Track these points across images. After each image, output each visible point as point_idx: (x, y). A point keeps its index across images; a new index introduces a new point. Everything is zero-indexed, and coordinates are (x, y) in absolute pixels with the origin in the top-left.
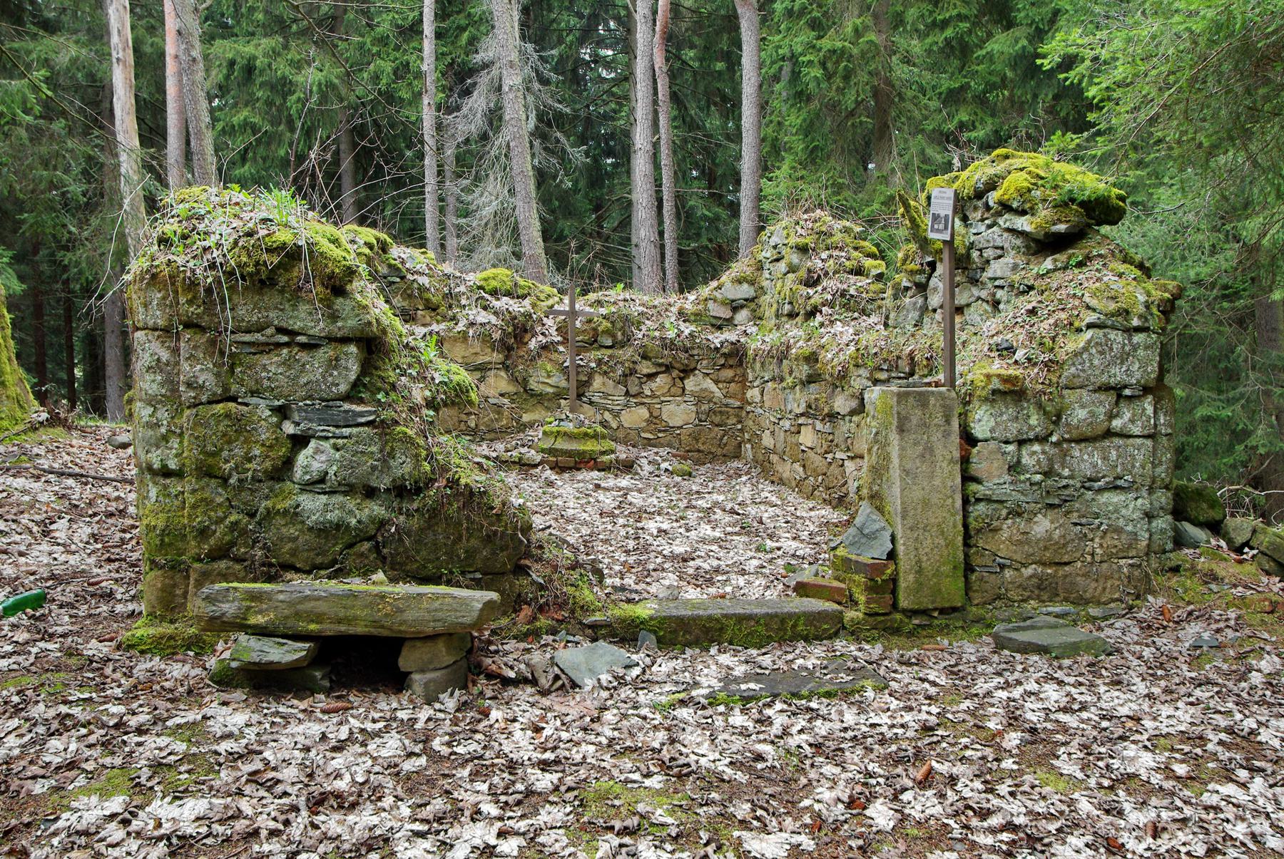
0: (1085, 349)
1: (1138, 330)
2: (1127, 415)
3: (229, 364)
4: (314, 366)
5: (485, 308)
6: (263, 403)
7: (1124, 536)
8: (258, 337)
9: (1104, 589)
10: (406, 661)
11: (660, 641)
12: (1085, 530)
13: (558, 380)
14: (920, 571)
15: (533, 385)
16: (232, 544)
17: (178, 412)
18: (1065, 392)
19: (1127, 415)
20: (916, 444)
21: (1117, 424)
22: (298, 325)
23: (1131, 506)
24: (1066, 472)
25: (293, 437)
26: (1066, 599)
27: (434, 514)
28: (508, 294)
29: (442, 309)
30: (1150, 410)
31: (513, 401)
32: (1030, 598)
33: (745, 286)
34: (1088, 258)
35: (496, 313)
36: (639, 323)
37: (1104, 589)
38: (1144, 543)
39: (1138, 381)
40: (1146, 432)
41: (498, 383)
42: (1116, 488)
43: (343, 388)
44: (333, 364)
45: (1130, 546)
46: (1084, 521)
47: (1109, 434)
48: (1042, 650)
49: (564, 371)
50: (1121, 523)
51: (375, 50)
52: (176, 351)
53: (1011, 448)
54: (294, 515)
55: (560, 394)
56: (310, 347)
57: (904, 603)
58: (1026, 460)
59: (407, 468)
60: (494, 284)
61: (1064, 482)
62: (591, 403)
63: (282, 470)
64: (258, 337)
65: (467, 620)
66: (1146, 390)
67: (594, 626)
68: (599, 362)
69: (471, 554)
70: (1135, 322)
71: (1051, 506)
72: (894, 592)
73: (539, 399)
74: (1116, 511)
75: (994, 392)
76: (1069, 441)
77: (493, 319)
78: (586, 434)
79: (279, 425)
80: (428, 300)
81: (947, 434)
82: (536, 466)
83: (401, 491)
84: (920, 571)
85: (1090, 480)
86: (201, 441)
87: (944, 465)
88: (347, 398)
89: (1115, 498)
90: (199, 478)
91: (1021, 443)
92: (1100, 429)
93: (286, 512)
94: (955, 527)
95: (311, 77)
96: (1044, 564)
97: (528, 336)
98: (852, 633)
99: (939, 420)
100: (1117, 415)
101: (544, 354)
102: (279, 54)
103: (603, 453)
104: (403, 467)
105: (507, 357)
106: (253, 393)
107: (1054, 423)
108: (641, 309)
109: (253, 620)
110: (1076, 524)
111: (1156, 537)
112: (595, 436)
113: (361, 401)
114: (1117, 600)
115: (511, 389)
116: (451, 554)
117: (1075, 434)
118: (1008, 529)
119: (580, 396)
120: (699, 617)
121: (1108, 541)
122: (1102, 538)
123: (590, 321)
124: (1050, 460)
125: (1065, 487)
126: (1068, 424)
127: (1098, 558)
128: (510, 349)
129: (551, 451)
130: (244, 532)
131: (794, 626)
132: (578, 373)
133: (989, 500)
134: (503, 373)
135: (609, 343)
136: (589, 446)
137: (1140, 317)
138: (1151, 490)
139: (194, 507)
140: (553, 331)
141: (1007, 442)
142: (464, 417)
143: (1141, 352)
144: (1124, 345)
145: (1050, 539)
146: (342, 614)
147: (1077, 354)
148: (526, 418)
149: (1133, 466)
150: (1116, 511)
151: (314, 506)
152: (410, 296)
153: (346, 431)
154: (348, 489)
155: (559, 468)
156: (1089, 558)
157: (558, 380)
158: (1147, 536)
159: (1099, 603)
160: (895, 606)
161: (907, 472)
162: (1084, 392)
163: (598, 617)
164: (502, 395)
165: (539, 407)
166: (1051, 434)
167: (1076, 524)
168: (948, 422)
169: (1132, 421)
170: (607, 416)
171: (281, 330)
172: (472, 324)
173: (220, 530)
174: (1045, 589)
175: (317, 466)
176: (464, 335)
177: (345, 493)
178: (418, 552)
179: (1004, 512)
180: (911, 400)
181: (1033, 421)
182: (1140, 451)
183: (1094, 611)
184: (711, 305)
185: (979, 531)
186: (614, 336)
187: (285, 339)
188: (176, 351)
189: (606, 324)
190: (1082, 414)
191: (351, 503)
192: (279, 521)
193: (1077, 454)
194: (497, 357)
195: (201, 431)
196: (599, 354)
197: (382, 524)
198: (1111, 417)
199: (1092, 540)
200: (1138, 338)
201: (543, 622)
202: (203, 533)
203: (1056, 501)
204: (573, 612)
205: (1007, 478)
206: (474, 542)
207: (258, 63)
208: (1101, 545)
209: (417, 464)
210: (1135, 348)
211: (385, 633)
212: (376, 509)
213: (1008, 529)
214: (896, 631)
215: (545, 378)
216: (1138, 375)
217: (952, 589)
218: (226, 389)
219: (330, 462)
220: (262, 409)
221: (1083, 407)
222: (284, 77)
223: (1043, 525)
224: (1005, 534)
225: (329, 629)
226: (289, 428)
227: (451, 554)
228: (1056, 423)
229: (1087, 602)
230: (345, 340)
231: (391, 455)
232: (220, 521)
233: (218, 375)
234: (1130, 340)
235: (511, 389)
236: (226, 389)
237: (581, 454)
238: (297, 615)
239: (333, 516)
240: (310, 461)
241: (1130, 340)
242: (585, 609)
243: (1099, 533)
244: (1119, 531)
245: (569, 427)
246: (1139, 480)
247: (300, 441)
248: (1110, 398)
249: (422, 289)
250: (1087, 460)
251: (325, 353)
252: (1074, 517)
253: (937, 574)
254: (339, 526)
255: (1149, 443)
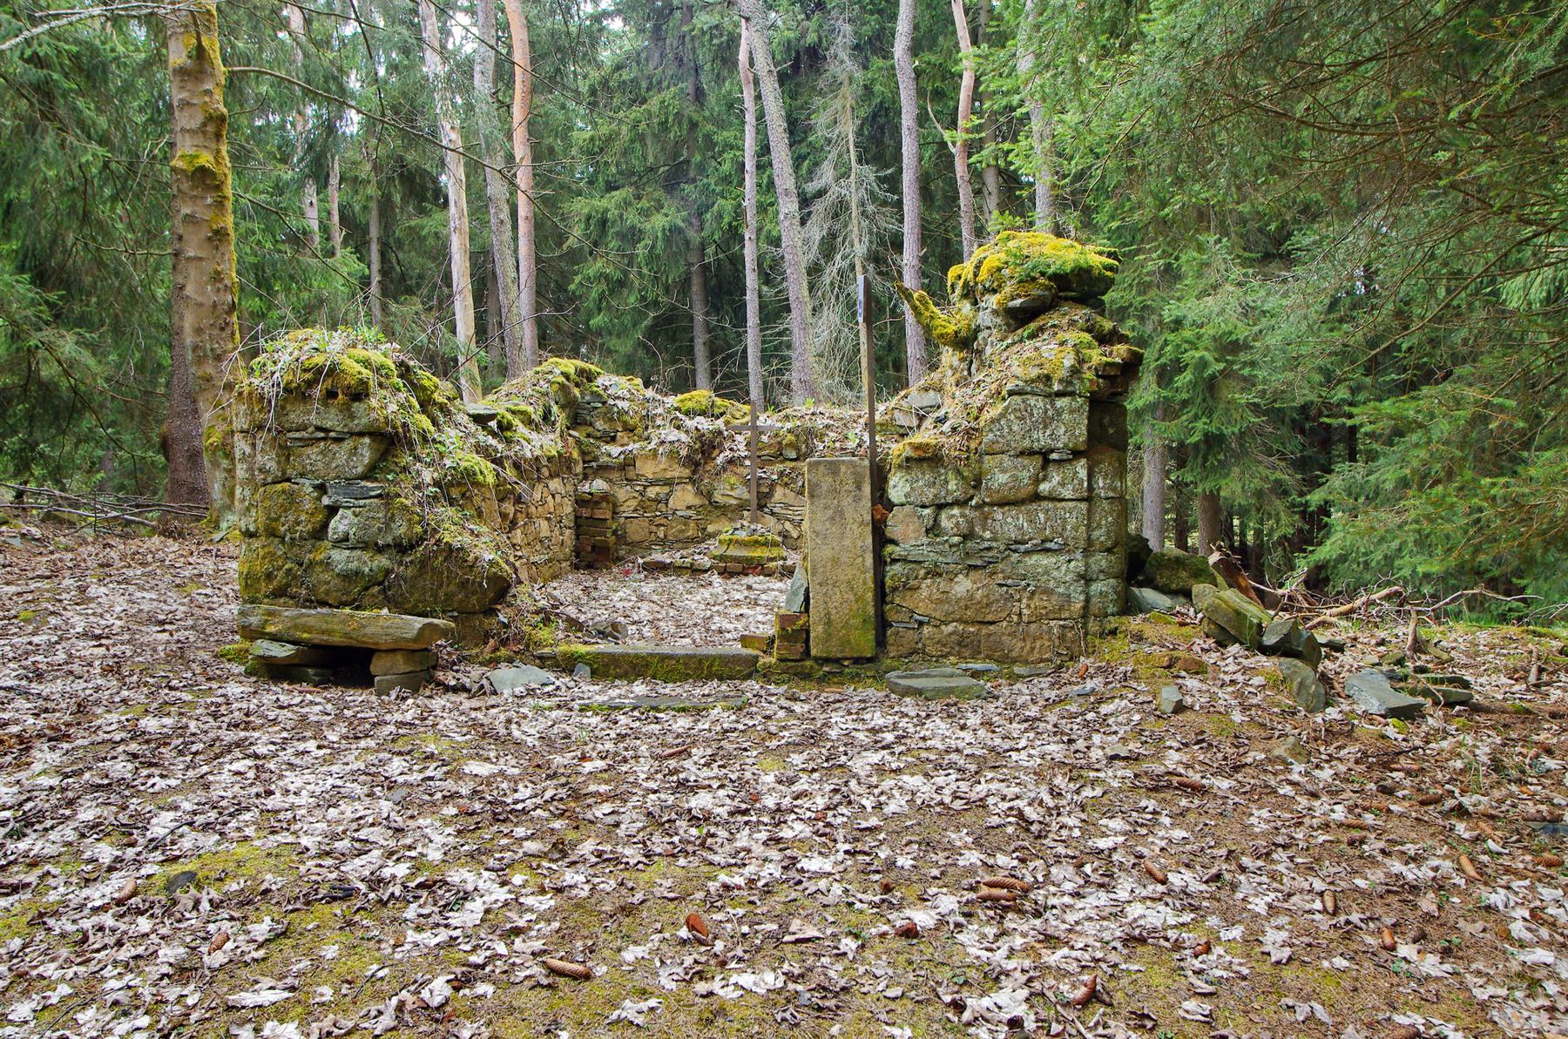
0: (1002, 415)
1: (1060, 394)
2: (1056, 479)
3: (285, 453)
4: (342, 452)
5: (678, 428)
6: (308, 482)
7: (1054, 598)
8: (304, 434)
9: (1033, 649)
10: (377, 666)
11: (593, 673)
12: (1011, 591)
13: (742, 493)
14: (829, 623)
15: (717, 497)
16: (288, 585)
17: (256, 490)
18: (987, 458)
19: (1056, 479)
20: (826, 507)
21: (1044, 487)
22: (329, 424)
23: (1063, 568)
24: (987, 535)
25: (327, 507)
26: (990, 657)
27: (424, 563)
28: (703, 413)
29: (639, 430)
30: (1083, 474)
31: (698, 513)
32: (949, 654)
33: (932, 393)
34: (1041, 329)
35: (687, 432)
36: (822, 435)
37: (1033, 649)
38: (1079, 606)
39: (1066, 445)
40: (1077, 495)
41: (685, 497)
42: (1048, 550)
43: (360, 470)
44: (354, 451)
45: (1061, 608)
46: (1010, 582)
47: (1036, 497)
48: (918, 692)
49: (747, 483)
50: (1052, 584)
51: (718, 189)
52: (254, 445)
53: (927, 511)
54: (327, 564)
55: (742, 506)
56: (338, 440)
57: (813, 652)
58: (945, 523)
59: (402, 530)
60: (689, 405)
61: (986, 544)
62: (773, 514)
63: (320, 532)
64: (304, 434)
65: (409, 636)
66: (1076, 454)
67: (541, 658)
68: (781, 474)
69: (449, 596)
70: (1056, 387)
71: (975, 567)
72: (807, 641)
73: (723, 510)
74: (1047, 572)
75: (908, 459)
76: (992, 504)
77: (684, 437)
78: (756, 542)
79: (319, 499)
80: (625, 423)
81: (857, 499)
82: (706, 571)
83: (402, 548)
84: (829, 623)
85: (1016, 542)
86: (267, 510)
87: (855, 527)
88: (364, 477)
89: (1045, 560)
90: (267, 537)
91: (940, 507)
92: (1023, 494)
93: (322, 562)
94: (865, 583)
95: (659, 222)
96: (966, 622)
97: (716, 452)
98: (765, 676)
99: (851, 486)
100: (1045, 479)
101: (730, 467)
102: (630, 204)
103: (772, 559)
104: (400, 529)
105: (694, 472)
106: (302, 475)
107: (974, 487)
108: (827, 422)
109: (271, 629)
110: (1001, 585)
111: (1094, 600)
112: (775, 544)
113: (376, 480)
114: (1048, 660)
115: (697, 501)
116: (435, 596)
117: (996, 497)
118: (927, 588)
119: (761, 507)
120: (628, 655)
121: (1036, 602)
122: (1030, 598)
123: (777, 435)
124: (971, 523)
125: (989, 549)
126: (988, 489)
127: (1025, 619)
128: (697, 464)
129: (722, 558)
130: (295, 577)
131: (711, 666)
132: (759, 485)
133: (905, 560)
134: (689, 487)
135: (793, 455)
136: (758, 553)
137: (1061, 381)
138: (1087, 551)
139: (264, 558)
140: (742, 447)
141: (924, 506)
142: (654, 528)
143: (1066, 416)
144: (1046, 411)
145: (971, 598)
146: (324, 627)
147: (993, 421)
148: (711, 528)
149: (1064, 529)
150: (1047, 572)
151: (340, 558)
152: (611, 420)
153: (362, 502)
154: (364, 545)
155: (726, 573)
156: (1015, 618)
157: (742, 493)
158: (1082, 597)
159: (1026, 662)
160: (807, 652)
161: (817, 534)
162: (1005, 458)
163: (547, 650)
164: (689, 508)
165: (723, 519)
166: (971, 498)
167: (1001, 585)
168: (859, 487)
169: (1062, 484)
170: (788, 525)
171: (319, 429)
172: (663, 442)
173: (281, 574)
174: (965, 646)
175: (342, 528)
176: (655, 452)
177: (363, 549)
178: (412, 594)
179: (922, 572)
180: (822, 468)
181: (952, 486)
182: (1073, 515)
183: (1017, 669)
184: (897, 414)
185: (895, 589)
186: (798, 449)
187: (322, 435)
188: (254, 445)
189: (790, 437)
190: (1002, 478)
191: (366, 556)
192: (318, 569)
193: (999, 517)
194: (687, 472)
195: (267, 503)
196: (780, 467)
197: (388, 572)
198: (1037, 481)
199: (1019, 601)
200: (1062, 403)
201: (503, 652)
202: (269, 576)
203: (979, 563)
204: (527, 646)
205: (925, 540)
206: (452, 588)
207: (609, 215)
208: (1028, 606)
209: (410, 527)
210: (1059, 413)
211: (354, 643)
212: (383, 561)
213: (927, 588)
214: (806, 676)
215: (730, 490)
216: (1064, 439)
217: (864, 642)
218: (284, 473)
219: (351, 525)
220: (307, 486)
221: (1004, 471)
222: (633, 227)
223: (963, 585)
224: (924, 592)
225: (317, 638)
226: (326, 501)
227: (435, 596)
228: (977, 487)
229: (1014, 661)
230: (361, 434)
231: (392, 519)
232: (279, 569)
233: (278, 463)
234: (1053, 404)
235: (697, 501)
236: (284, 473)
237: (749, 560)
238: (296, 627)
239: (353, 566)
240: (341, 524)
241: (1053, 404)
242: (538, 644)
243: (1026, 594)
244: (1049, 592)
245: (742, 535)
246: (1071, 543)
247: (332, 510)
248: (1032, 465)
249: (622, 412)
250: (1011, 523)
251: (348, 444)
252: (999, 578)
253: (846, 625)
254: (357, 573)
255: (1083, 506)
